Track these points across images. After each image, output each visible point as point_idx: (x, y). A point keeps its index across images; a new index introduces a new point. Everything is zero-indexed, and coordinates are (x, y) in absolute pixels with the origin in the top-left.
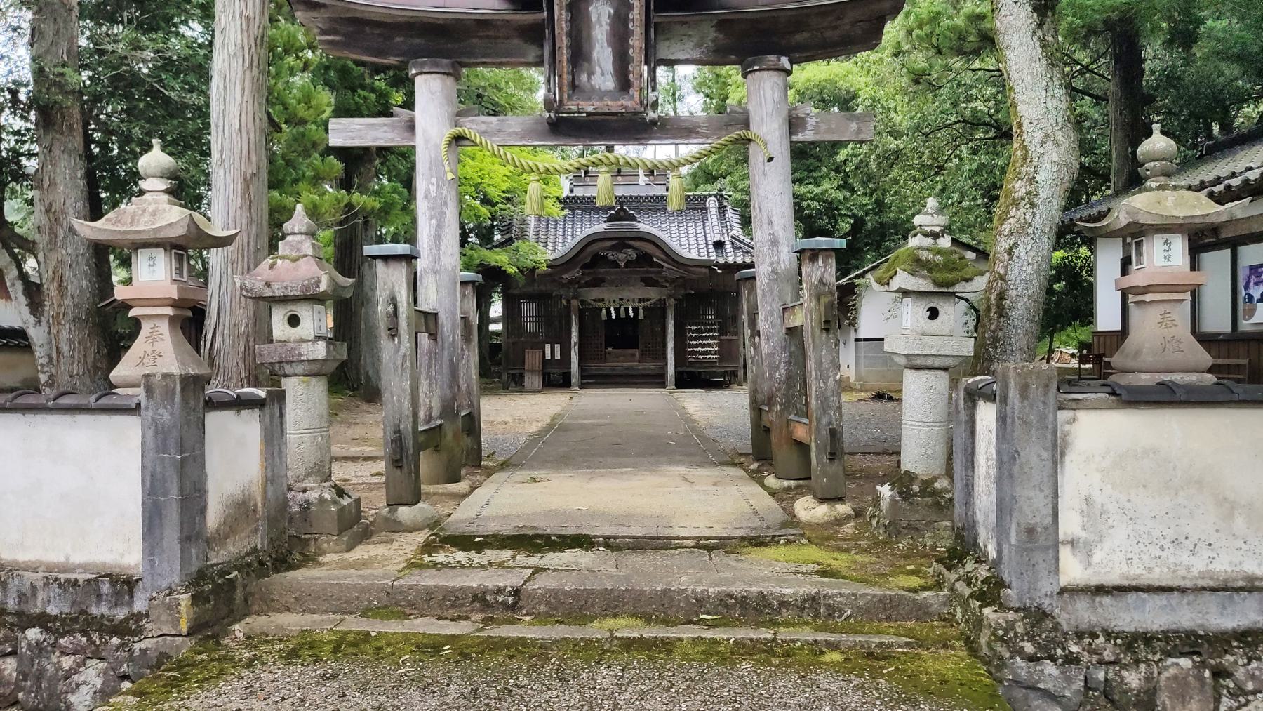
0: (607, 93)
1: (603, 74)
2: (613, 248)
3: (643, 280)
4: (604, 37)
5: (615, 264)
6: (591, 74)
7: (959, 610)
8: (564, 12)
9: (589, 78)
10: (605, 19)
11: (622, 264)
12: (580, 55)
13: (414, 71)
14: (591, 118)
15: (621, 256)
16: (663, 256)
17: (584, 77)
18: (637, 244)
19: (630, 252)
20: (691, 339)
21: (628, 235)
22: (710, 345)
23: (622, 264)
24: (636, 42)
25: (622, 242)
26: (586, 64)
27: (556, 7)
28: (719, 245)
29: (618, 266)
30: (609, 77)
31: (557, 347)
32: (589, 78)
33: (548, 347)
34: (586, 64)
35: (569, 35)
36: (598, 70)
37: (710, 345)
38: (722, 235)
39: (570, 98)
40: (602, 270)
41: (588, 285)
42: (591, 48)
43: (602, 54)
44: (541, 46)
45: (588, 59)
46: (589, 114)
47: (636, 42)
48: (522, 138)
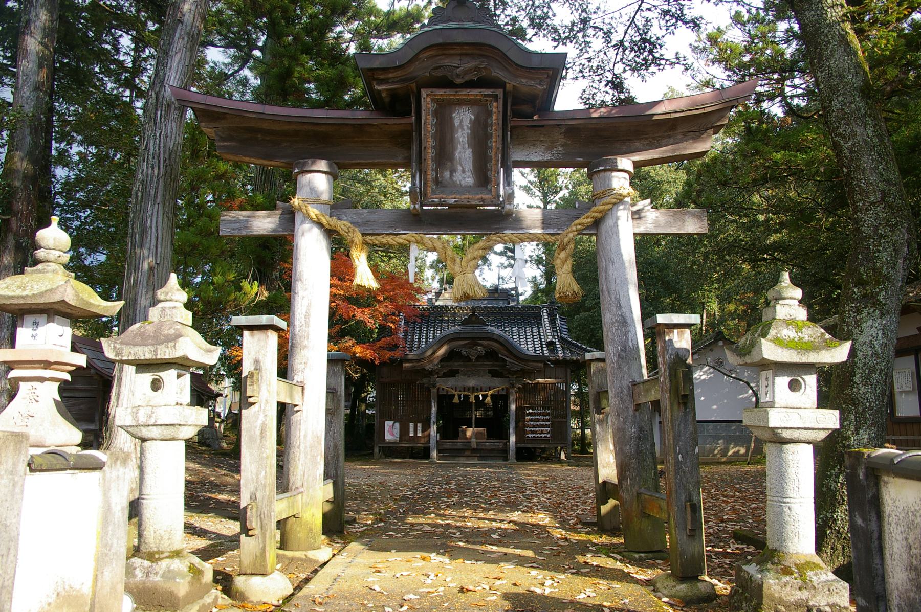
0: (467, 189)
1: (464, 172)
2: (464, 346)
3: (490, 372)
4: (466, 140)
5: (468, 359)
6: (453, 171)
7: (369, 354)
8: (429, 117)
9: (451, 175)
10: (466, 123)
11: (473, 358)
12: (444, 155)
13: (296, 171)
14: (453, 210)
15: (472, 352)
16: (506, 353)
17: (447, 174)
18: (485, 343)
19: (479, 348)
20: (548, 420)
21: (478, 335)
22: (531, 420)
23: (473, 358)
24: (495, 143)
25: (474, 341)
26: (449, 163)
27: (423, 113)
28: (550, 344)
29: (470, 360)
30: (469, 174)
31: (419, 425)
32: (451, 175)
33: (412, 425)
34: (449, 163)
35: (434, 137)
36: (460, 168)
37: (531, 420)
38: (553, 337)
39: (434, 192)
40: (456, 364)
41: (445, 375)
42: (454, 149)
43: (464, 155)
44: (410, 148)
45: (451, 158)
46: (451, 206)
47: (495, 143)
48: (390, 227)
